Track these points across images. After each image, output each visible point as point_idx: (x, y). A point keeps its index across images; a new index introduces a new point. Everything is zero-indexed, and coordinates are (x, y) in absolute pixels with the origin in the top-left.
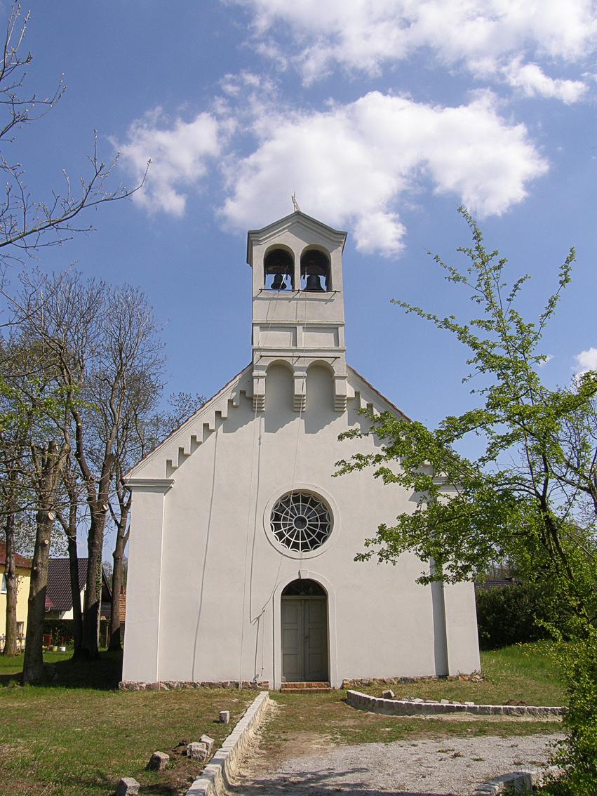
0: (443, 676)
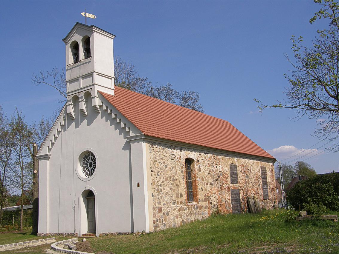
0: (133, 232)
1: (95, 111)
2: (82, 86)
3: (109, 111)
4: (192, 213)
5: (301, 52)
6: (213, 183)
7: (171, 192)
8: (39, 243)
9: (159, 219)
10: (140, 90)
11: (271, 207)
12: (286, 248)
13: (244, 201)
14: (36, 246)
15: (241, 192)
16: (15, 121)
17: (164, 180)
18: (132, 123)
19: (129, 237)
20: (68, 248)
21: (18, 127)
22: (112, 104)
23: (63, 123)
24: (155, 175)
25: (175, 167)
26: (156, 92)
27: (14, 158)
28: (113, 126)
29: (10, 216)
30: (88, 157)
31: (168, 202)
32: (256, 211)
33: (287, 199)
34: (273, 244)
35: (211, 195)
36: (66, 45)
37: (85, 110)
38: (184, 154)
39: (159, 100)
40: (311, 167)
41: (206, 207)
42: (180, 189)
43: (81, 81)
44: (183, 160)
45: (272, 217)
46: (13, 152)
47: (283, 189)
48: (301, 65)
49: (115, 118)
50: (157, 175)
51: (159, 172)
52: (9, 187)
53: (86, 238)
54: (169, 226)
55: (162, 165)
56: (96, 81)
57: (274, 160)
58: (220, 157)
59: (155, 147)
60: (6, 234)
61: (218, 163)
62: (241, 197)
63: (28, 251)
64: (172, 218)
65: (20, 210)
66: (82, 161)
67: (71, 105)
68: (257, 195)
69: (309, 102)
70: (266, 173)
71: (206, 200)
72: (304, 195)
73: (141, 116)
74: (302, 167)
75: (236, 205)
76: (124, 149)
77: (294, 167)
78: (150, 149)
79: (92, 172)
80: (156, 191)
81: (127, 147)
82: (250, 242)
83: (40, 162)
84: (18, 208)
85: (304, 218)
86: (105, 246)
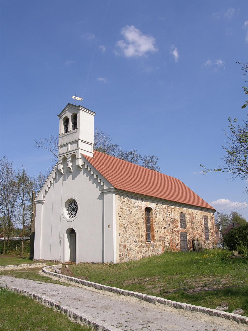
0: (103, 263)
1: (78, 169)
2: (69, 150)
3: (89, 169)
4: (149, 250)
5: (236, 130)
6: (166, 227)
7: (133, 233)
8: (34, 266)
9: (124, 254)
10: (113, 154)
11: (211, 246)
12: (222, 280)
13: (190, 242)
14: (32, 268)
15: (188, 234)
16: (20, 174)
17: (129, 223)
18: (106, 179)
19: (101, 266)
20: (55, 272)
21: (23, 179)
22: (91, 164)
23: (54, 177)
24: (122, 219)
25: (138, 213)
26: (124, 156)
27: (19, 201)
28: (92, 181)
29: (15, 244)
30: (72, 204)
31: (131, 241)
32: (199, 249)
33: (223, 241)
34: (212, 277)
35: (165, 236)
36: (60, 119)
37: (71, 168)
38: (145, 204)
39: (127, 162)
40: (242, 217)
41: (160, 246)
42: (141, 231)
43: (69, 146)
44: (144, 209)
45: (211, 255)
46: (18, 197)
47: (220, 233)
48: (235, 139)
49: (93, 175)
50: (123, 219)
51: (125, 217)
52: (14, 223)
53: (68, 265)
54: (132, 259)
55: (128, 212)
56: (80, 147)
57: (214, 211)
58: (172, 207)
59: (122, 198)
60: (11, 257)
61: (170, 212)
62: (188, 239)
63: (26, 271)
64: (134, 253)
65: (22, 240)
66: (67, 206)
67: (61, 164)
68: (200, 237)
69: (241, 167)
70: (208, 220)
71: (160, 240)
72: (237, 239)
73: (131, 186)
74: (235, 217)
75: (184, 245)
76: (99, 198)
77: (229, 216)
78: (119, 200)
79: (74, 215)
80: (122, 232)
81: (101, 197)
82: (193, 275)
83: (37, 205)
84: (20, 238)
85: (236, 257)
86: (82, 272)
